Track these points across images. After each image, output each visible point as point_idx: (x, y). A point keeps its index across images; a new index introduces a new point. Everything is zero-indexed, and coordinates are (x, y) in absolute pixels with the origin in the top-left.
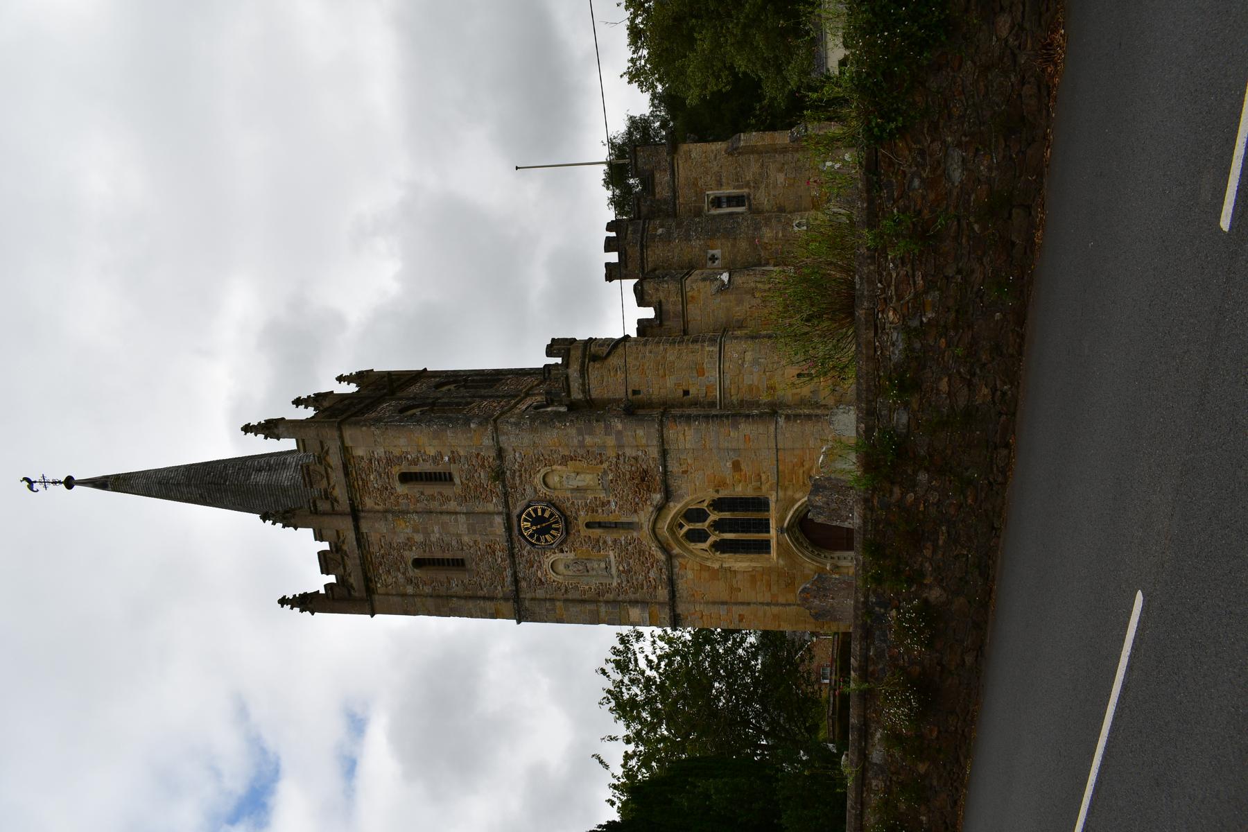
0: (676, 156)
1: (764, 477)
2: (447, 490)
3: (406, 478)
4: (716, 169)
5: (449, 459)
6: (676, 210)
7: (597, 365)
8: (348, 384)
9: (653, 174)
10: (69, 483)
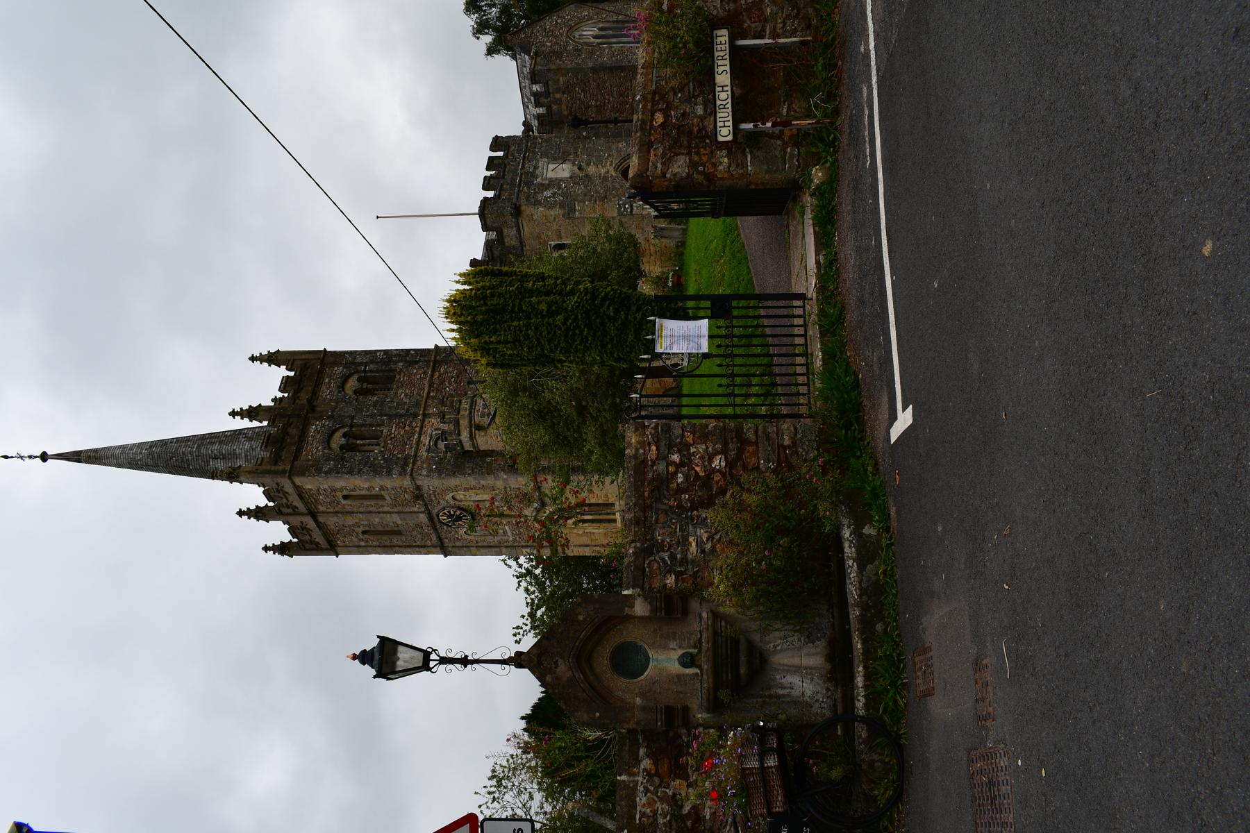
0: (520, 219)
1: (610, 496)
2: (380, 503)
3: (345, 497)
4: (555, 227)
5: (379, 489)
7: (482, 434)
8: (276, 397)
9: (502, 230)
10: (44, 457)
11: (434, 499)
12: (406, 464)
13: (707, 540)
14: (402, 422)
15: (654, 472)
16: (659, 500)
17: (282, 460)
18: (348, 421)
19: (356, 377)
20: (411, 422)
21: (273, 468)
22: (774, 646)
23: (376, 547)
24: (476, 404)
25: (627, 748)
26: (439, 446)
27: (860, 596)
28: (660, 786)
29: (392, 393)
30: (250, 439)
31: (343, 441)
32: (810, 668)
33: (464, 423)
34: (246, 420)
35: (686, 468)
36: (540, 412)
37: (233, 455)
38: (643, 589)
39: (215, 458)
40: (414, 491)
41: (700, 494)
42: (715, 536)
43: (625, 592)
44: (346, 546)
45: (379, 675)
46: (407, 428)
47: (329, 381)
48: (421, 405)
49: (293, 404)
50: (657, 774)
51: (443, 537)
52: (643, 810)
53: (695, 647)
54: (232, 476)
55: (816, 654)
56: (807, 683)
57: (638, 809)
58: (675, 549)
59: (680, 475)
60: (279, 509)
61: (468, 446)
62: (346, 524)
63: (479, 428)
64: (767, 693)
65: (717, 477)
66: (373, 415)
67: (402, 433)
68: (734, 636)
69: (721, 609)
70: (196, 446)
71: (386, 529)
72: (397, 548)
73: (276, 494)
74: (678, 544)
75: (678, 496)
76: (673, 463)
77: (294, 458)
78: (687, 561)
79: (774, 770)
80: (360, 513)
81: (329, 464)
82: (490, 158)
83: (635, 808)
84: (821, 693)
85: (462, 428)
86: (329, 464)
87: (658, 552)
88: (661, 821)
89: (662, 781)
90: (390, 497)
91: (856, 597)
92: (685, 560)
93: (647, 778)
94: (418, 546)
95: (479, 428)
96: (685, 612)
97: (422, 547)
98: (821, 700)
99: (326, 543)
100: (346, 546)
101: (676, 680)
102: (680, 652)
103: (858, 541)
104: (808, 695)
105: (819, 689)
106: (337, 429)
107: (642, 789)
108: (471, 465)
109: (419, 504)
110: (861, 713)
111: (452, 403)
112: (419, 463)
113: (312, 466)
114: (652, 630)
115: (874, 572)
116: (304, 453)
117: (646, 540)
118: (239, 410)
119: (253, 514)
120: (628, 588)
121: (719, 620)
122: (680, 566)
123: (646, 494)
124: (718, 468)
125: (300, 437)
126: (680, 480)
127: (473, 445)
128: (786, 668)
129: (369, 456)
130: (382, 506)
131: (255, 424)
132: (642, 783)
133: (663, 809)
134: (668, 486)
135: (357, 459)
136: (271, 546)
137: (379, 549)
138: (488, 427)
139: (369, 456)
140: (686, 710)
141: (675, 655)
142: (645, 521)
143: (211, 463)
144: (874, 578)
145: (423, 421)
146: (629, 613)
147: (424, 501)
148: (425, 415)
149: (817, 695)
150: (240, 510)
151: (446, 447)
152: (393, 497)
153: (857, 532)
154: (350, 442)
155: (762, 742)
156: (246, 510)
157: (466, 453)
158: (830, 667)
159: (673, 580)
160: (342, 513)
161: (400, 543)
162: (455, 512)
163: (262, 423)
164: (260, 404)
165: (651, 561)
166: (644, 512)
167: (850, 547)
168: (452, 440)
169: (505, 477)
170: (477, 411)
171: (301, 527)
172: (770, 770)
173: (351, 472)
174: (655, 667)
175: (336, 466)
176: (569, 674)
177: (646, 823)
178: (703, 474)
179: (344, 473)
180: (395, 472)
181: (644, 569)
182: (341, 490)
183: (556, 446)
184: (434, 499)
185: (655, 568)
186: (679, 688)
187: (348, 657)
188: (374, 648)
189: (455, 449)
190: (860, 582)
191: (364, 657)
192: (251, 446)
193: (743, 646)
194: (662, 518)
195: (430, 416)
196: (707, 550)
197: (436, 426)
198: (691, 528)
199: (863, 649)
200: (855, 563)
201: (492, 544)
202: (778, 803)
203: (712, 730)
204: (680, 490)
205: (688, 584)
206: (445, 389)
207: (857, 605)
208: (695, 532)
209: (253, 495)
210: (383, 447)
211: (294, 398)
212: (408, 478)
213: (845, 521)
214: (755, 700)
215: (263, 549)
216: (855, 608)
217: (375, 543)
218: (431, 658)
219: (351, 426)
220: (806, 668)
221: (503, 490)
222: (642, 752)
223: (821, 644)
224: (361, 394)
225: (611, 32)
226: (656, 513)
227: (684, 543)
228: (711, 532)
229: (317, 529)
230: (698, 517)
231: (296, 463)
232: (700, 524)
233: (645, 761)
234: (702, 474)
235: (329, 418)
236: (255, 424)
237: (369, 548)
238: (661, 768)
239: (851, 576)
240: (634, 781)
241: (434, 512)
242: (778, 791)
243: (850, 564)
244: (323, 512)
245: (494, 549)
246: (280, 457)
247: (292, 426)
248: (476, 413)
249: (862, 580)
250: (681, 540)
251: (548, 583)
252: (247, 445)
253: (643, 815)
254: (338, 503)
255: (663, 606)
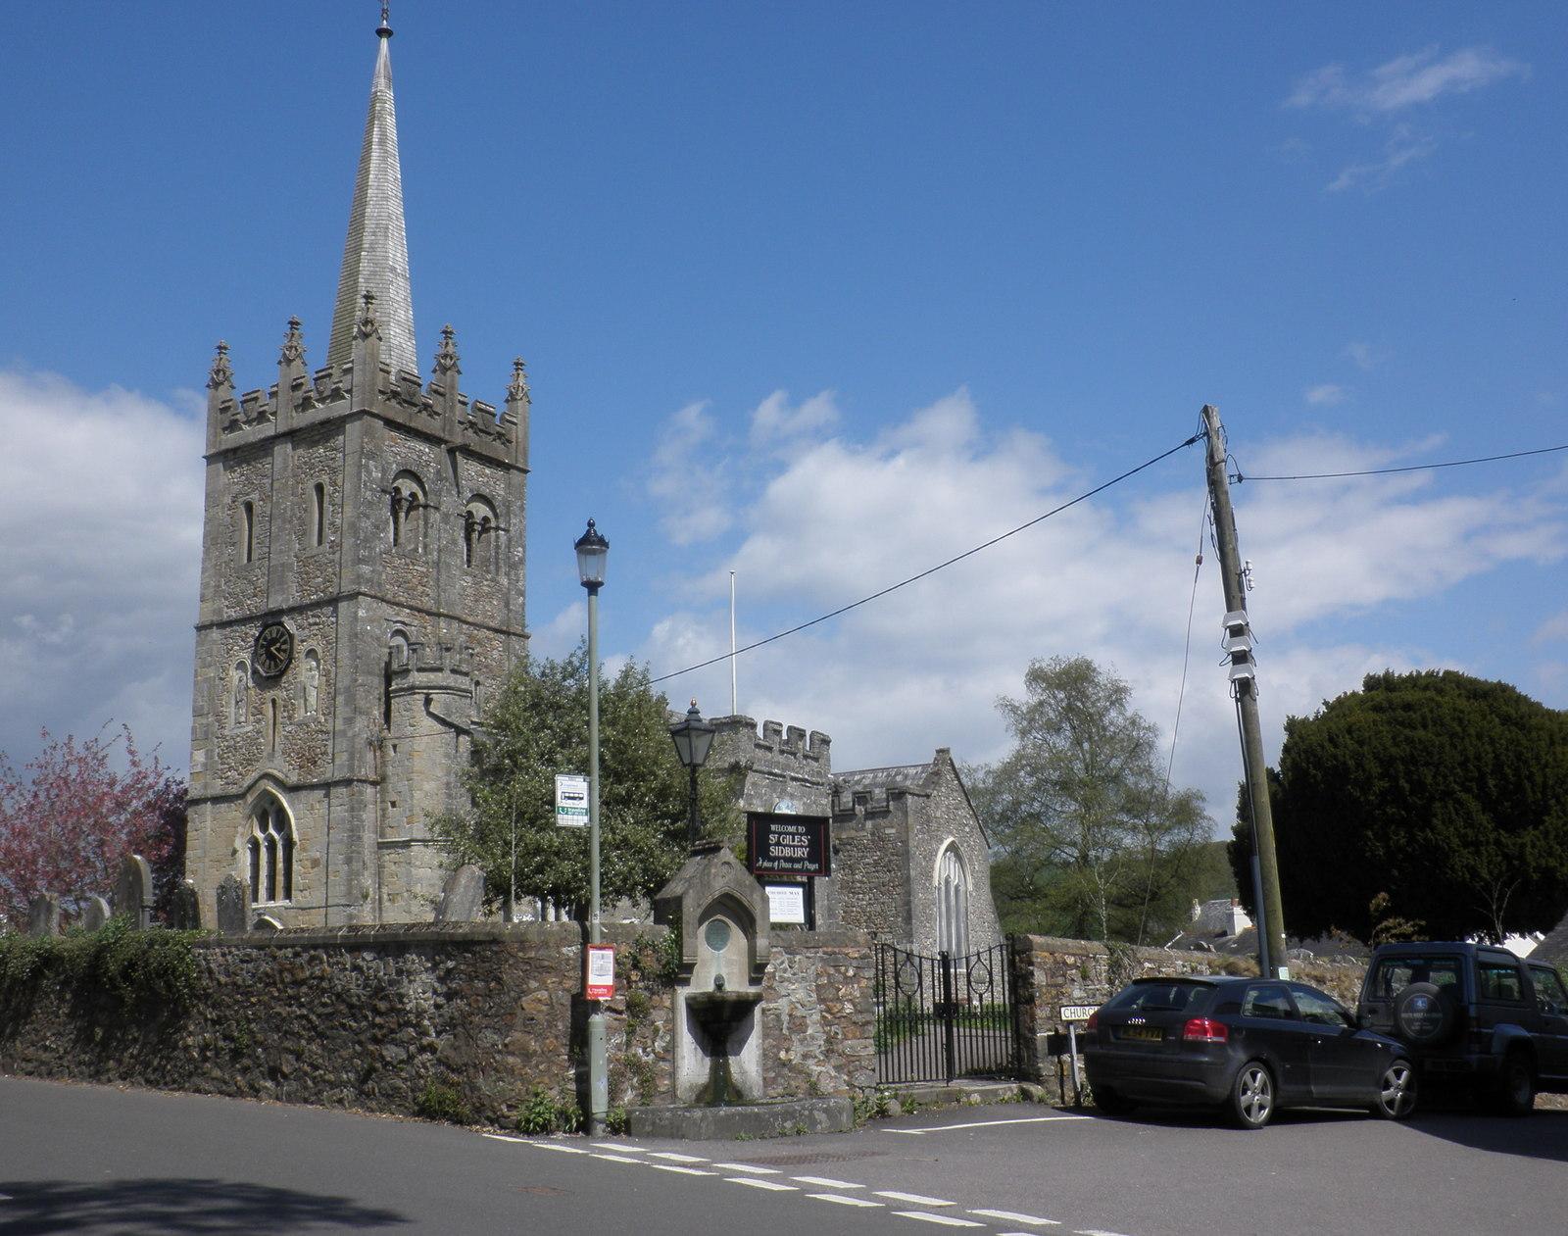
19: (490, 515)
47: (486, 476)
76: (847, 971)
82: (805, 731)
95: (428, 701)
225: (953, 902)
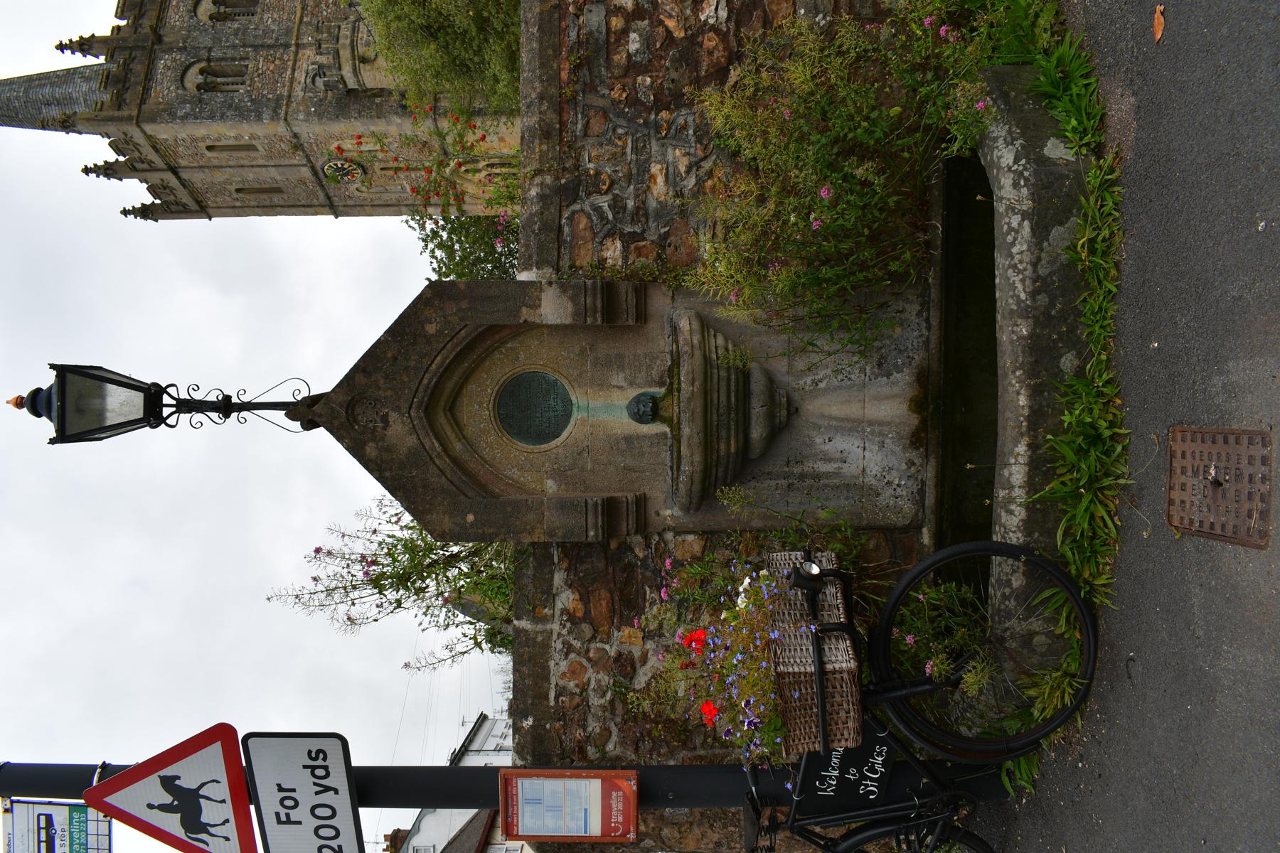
2: (253, 154)
3: (209, 148)
5: (250, 137)
6: (636, 297)
7: (368, 67)
11: (316, 149)
12: (278, 106)
13: (688, 172)
14: (271, 55)
15: (579, 30)
16: (590, 88)
17: (126, 104)
18: (204, 54)
20: (282, 55)
21: (116, 114)
22: (813, 381)
23: (254, 207)
24: (358, 30)
25: (530, 572)
26: (317, 84)
27: (1033, 294)
28: (593, 638)
29: (256, 18)
30: (87, 79)
31: (200, 79)
32: (881, 423)
33: (345, 54)
34: (78, 54)
35: (646, 22)
36: (428, 27)
37: (70, 100)
38: (558, 270)
39: (48, 104)
40: (291, 139)
41: (674, 75)
42: (702, 164)
43: (523, 276)
44: (220, 207)
45: (63, 436)
46: (277, 62)
48: (293, 32)
49: (135, 33)
50: (587, 617)
51: (332, 195)
52: (561, 683)
53: (661, 384)
54: (67, 125)
55: (895, 396)
56: (871, 451)
57: (553, 681)
58: (622, 189)
59: (633, 36)
60: (132, 165)
61: (352, 84)
62: (216, 181)
63: (364, 60)
64: (797, 470)
65: (710, 41)
66: (234, 47)
67: (271, 68)
68: (741, 365)
69: (721, 313)
70: (23, 89)
71: (264, 186)
72: (279, 208)
73: (126, 146)
74: (629, 178)
75: (628, 80)
77: (141, 101)
78: (646, 215)
79: (845, 676)
80: (230, 167)
81: (185, 108)
83: (547, 678)
84: (898, 470)
85: (343, 60)
86: (185, 108)
87: (589, 195)
88: (595, 701)
89: (596, 631)
90: (264, 148)
91: (1023, 296)
92: (641, 212)
93: (568, 625)
94: (304, 206)
95: (364, 60)
96: (642, 316)
97: (308, 206)
98: (896, 482)
99: (194, 203)
100: (220, 207)
101: (623, 446)
102: (633, 393)
103: (1036, 173)
104: (874, 473)
105: (893, 462)
106: (194, 63)
107: (559, 646)
108: (357, 106)
109: (299, 155)
110: (1015, 538)
111: (329, 29)
112: (294, 105)
113: (164, 110)
114: (577, 350)
115: (1067, 243)
116: (153, 95)
117: (564, 169)
118: (68, 43)
119: (102, 170)
120: (527, 267)
121: (712, 332)
122: (633, 222)
123: (564, 75)
124: (711, 21)
125: (147, 75)
126: (633, 47)
127: (359, 81)
128: (834, 423)
129: (232, 97)
130: (255, 158)
131: (90, 60)
132: (559, 635)
133: (598, 681)
134: (608, 59)
135: (218, 101)
136: (131, 209)
137: (257, 210)
138: (375, 59)
139: (232, 97)
140: (641, 502)
141: (622, 399)
142: (561, 131)
143: (44, 111)
144: (1064, 258)
145: (296, 53)
146: (531, 319)
147: (304, 151)
148: (297, 45)
149: (889, 472)
150: (86, 166)
151: (326, 84)
152: (266, 147)
153: (1031, 152)
154: (208, 80)
155: (814, 607)
156: (92, 166)
157: (350, 92)
158: (916, 422)
159: (618, 252)
160: (208, 167)
161: (282, 203)
162: (342, 165)
163: (97, 57)
164: (93, 35)
165: (574, 213)
166: (560, 112)
167: (1016, 185)
168: (332, 76)
169: (399, 121)
170: (361, 39)
171: (163, 186)
172: (838, 676)
173: (212, 117)
174: (584, 421)
175: (193, 110)
176: (411, 441)
177: (567, 705)
178: (682, 35)
179: (203, 118)
180: (265, 116)
181: (560, 228)
182: (203, 139)
183: (453, 75)
184: (316, 149)
185: (581, 226)
186: (629, 462)
187: (8, 402)
188: (52, 385)
189: (337, 88)
190: (1035, 265)
191: (35, 403)
192: (90, 88)
193: (758, 384)
194: (596, 126)
195: (304, 46)
196: (686, 191)
197: (312, 59)
198: (655, 146)
199: (1030, 407)
200: (1026, 223)
201: (389, 203)
202: (846, 733)
203: (690, 538)
204: (633, 67)
205: (648, 261)
206: (322, 12)
207: (1024, 313)
208: (664, 155)
209: (98, 149)
210: (250, 86)
211: (135, 26)
212: (282, 123)
213: (999, 131)
214: (773, 483)
215: (121, 212)
216: (1019, 321)
217: (252, 203)
218: (164, 402)
219: (209, 60)
220: (871, 423)
221: (398, 137)
222: (558, 578)
223: (903, 381)
224: (218, 20)
226: (584, 115)
227: (640, 175)
228: (695, 155)
229: (182, 187)
230: (670, 124)
231: (143, 107)
232: (674, 138)
233: (564, 595)
234: (679, 34)
235: (180, 49)
236: (90, 60)
237: (245, 209)
238: (596, 608)
239: (1014, 250)
240: (544, 631)
241: (318, 165)
242: (848, 712)
243: (1015, 224)
244: (186, 167)
245: (392, 209)
246: (124, 100)
247: (135, 61)
248: (359, 41)
249: (1039, 259)
250: (634, 171)
251: (457, 247)
252: (85, 88)
253: (561, 692)
254: (202, 156)
255: (599, 305)
